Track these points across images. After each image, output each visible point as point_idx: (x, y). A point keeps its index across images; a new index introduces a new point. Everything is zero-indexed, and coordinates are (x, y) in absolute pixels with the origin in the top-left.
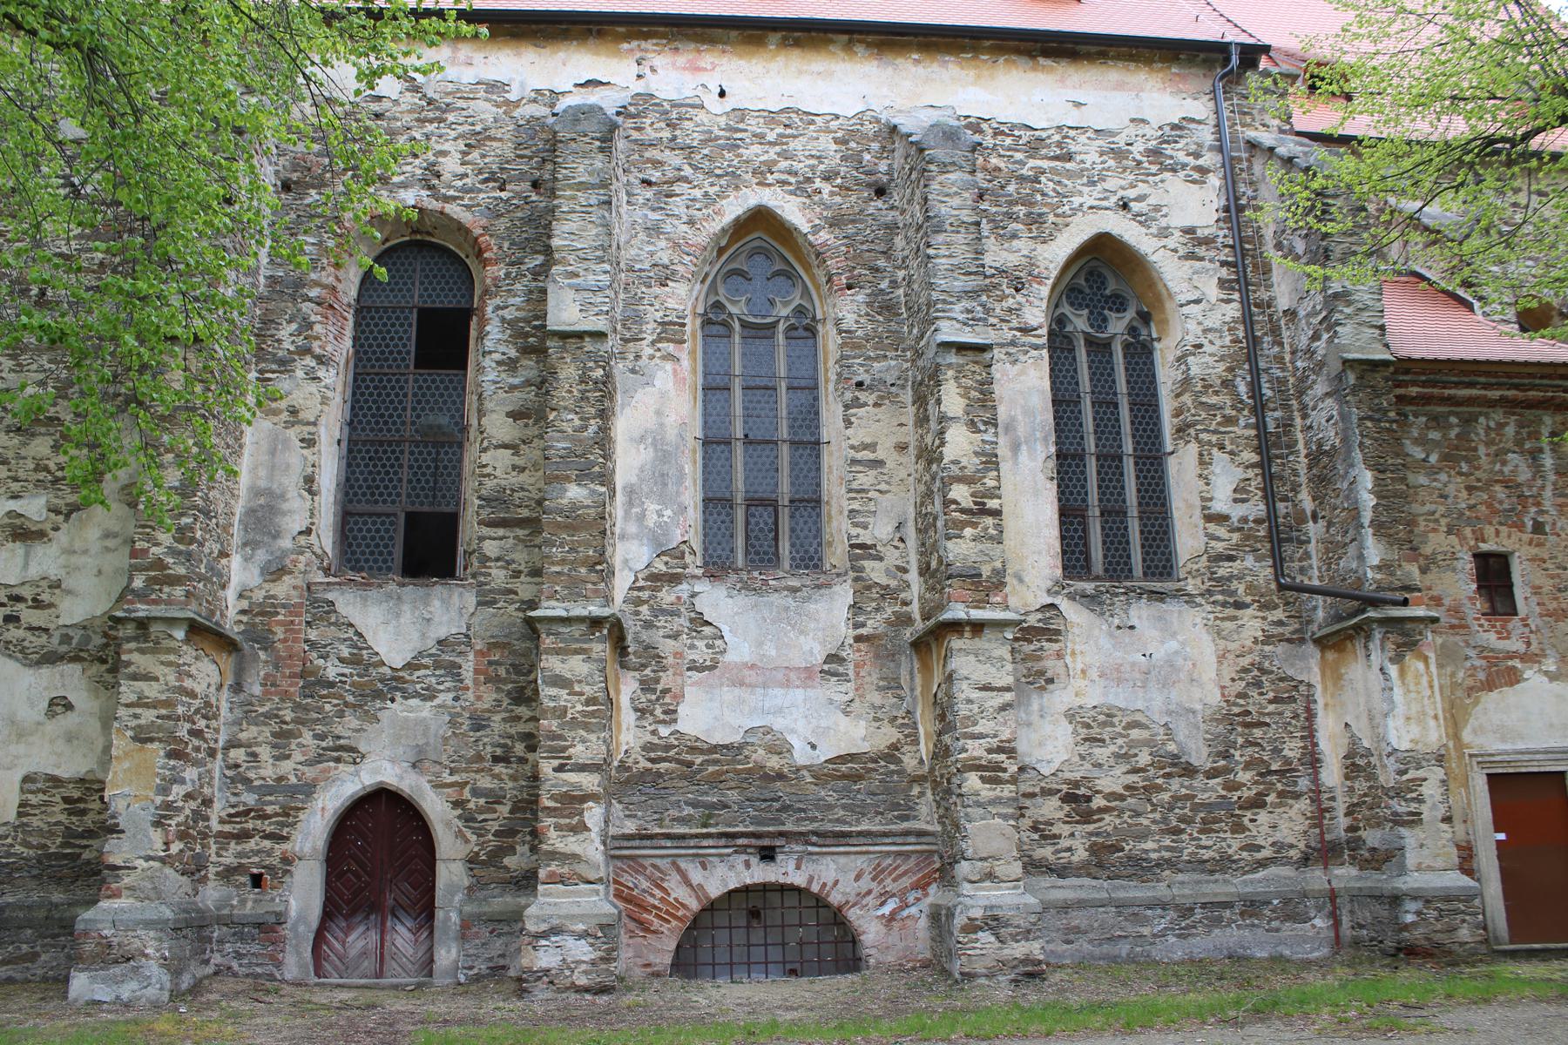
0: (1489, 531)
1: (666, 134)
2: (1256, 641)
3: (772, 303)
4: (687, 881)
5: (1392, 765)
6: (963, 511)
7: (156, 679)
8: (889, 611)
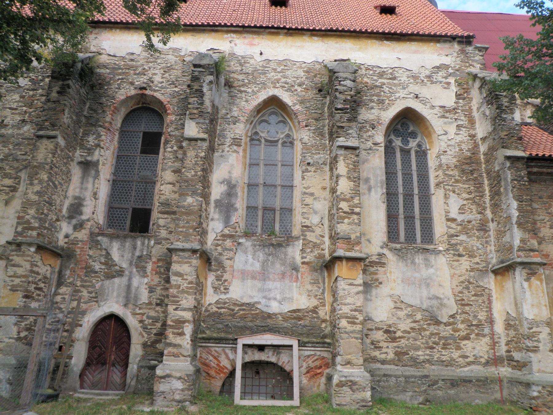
1: (239, 68)
2: (467, 270)
3: (277, 133)
4: (227, 357)
5: (526, 325)
6: (345, 212)
7: (22, 267)
8: (316, 252)
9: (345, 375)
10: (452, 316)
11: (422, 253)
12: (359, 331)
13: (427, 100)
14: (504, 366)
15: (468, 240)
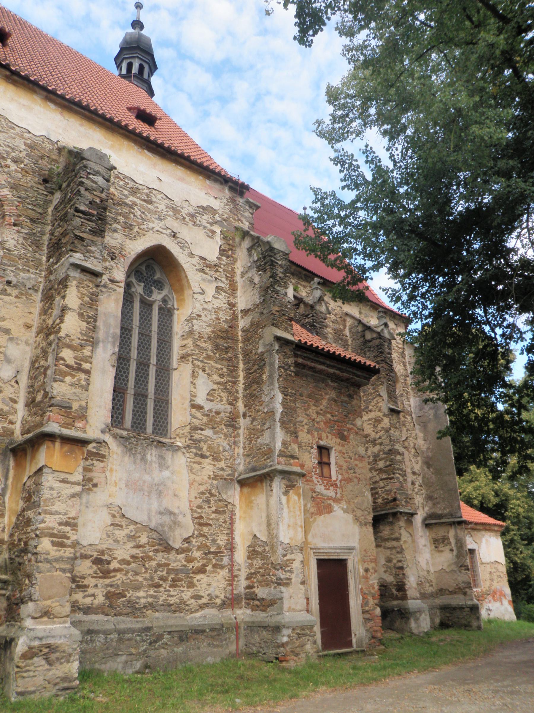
0: (324, 435)
6: (67, 366)
9: (40, 635)
10: (187, 540)
11: (156, 447)
12: (68, 558)
13: (186, 245)
14: (241, 608)
15: (215, 437)
